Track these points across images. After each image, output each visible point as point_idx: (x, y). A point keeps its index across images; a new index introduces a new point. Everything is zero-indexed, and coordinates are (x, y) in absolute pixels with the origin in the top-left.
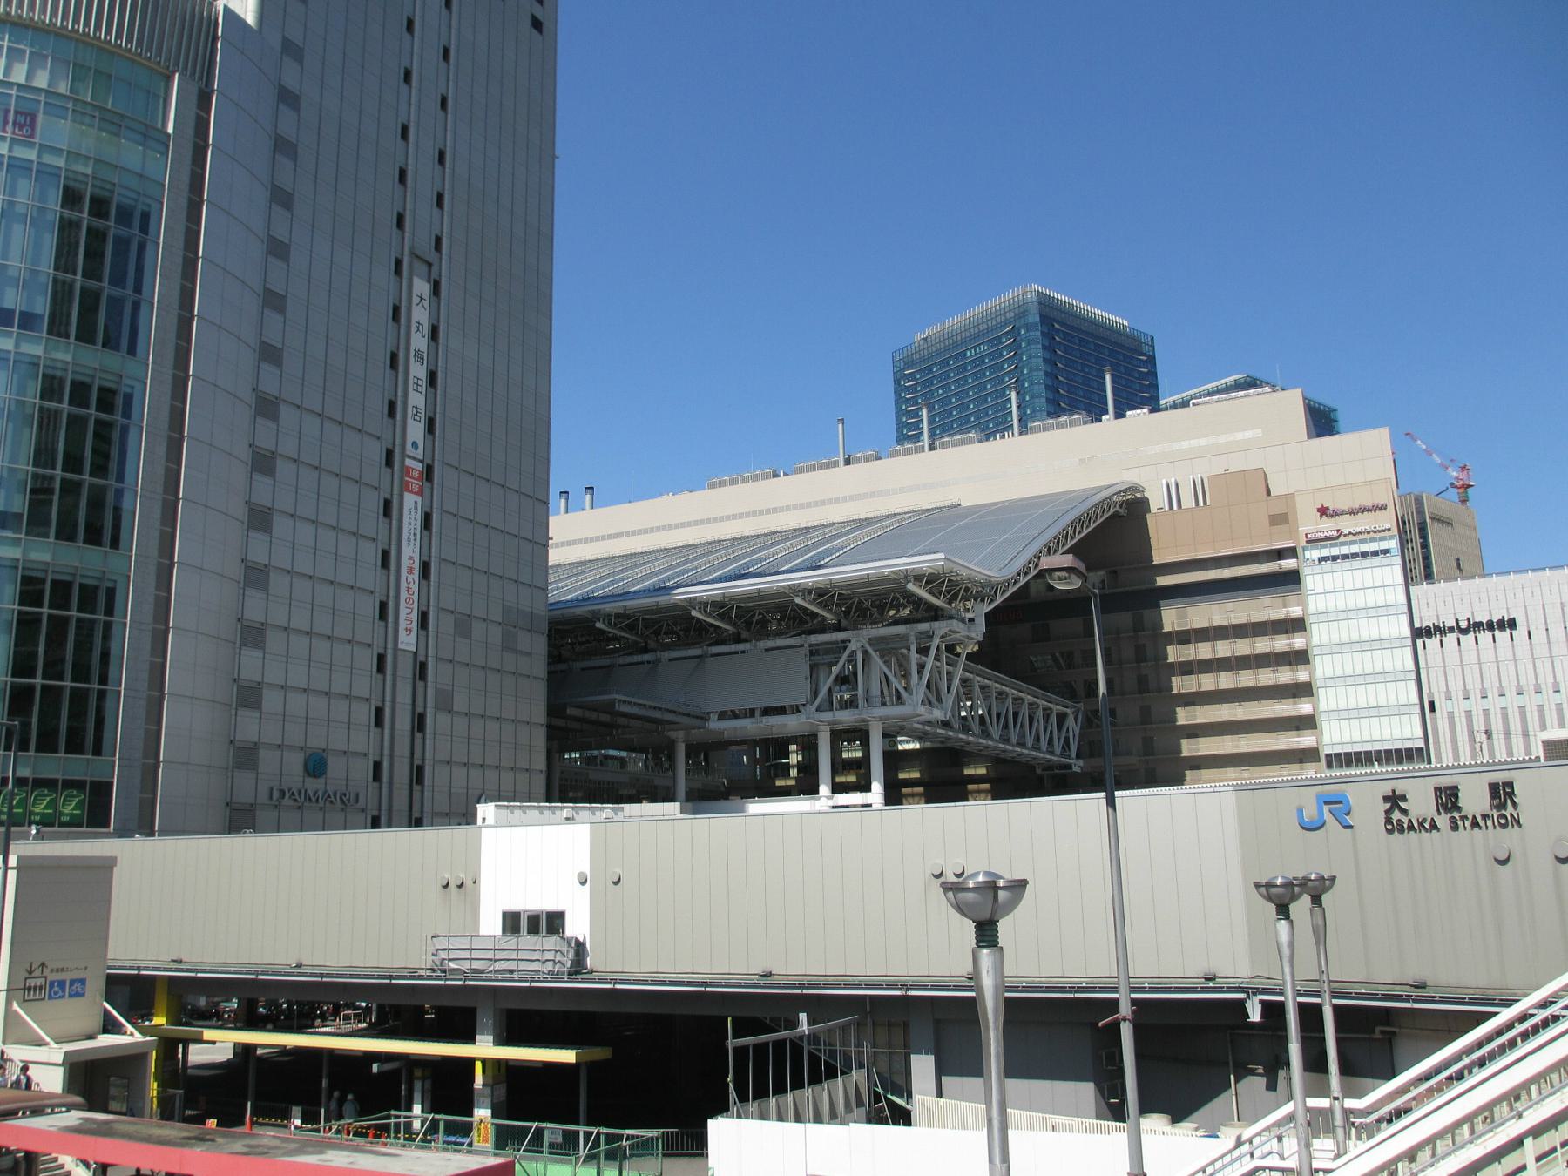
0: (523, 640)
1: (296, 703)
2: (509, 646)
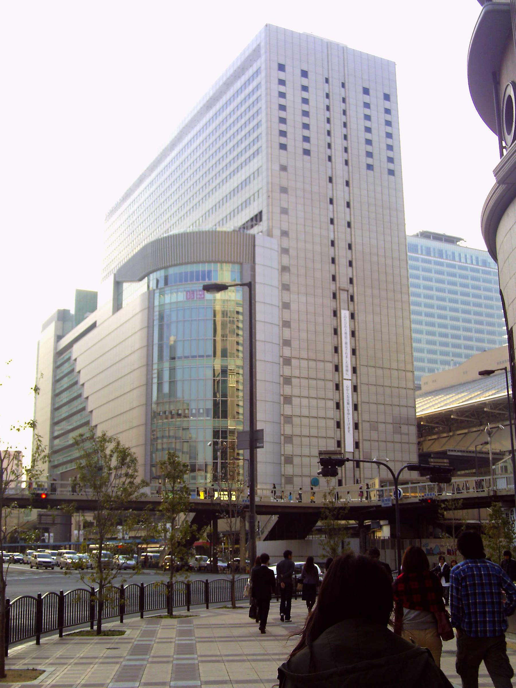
0: (404, 429)
1: (305, 421)
2: (397, 431)
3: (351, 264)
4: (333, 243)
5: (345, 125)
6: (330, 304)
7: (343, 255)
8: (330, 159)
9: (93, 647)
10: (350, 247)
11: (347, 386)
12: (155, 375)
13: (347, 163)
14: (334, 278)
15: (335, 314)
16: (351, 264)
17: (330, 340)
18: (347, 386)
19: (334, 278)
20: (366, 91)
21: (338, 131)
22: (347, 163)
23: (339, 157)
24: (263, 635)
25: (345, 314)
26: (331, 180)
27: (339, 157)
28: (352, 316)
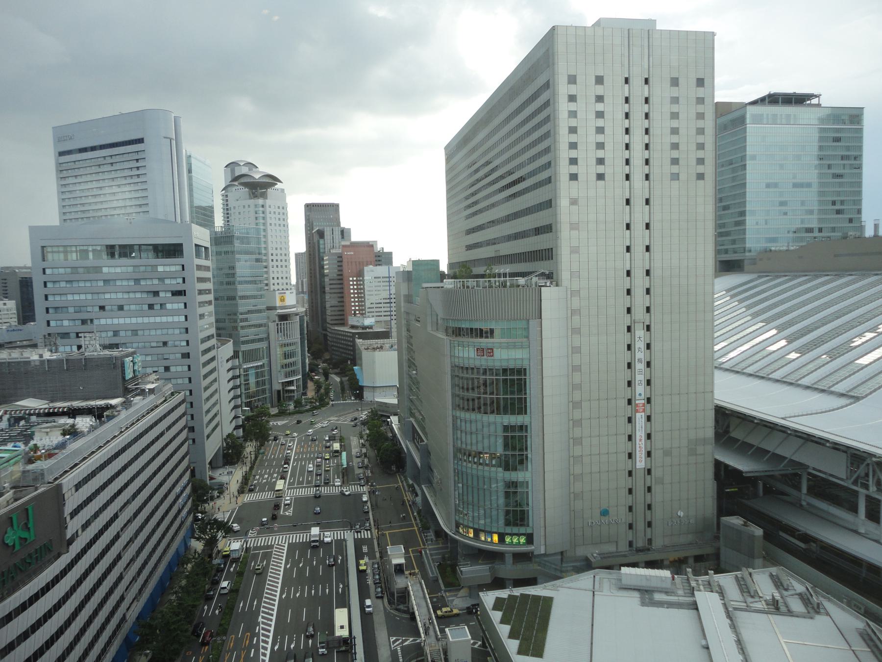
3: (648, 291)
4: (628, 273)
5: (647, 131)
6: (626, 338)
7: (639, 282)
8: (628, 177)
9: (124, 261)
10: (648, 273)
11: (640, 435)
12: (132, 295)
13: (647, 177)
14: (629, 310)
15: (630, 420)
16: (648, 291)
17: (624, 446)
18: (640, 435)
19: (629, 310)
20: (675, 82)
21: (638, 139)
22: (647, 177)
23: (638, 170)
24: (553, 180)
25: (640, 418)
26: (628, 202)
27: (638, 170)
28: (649, 418)
